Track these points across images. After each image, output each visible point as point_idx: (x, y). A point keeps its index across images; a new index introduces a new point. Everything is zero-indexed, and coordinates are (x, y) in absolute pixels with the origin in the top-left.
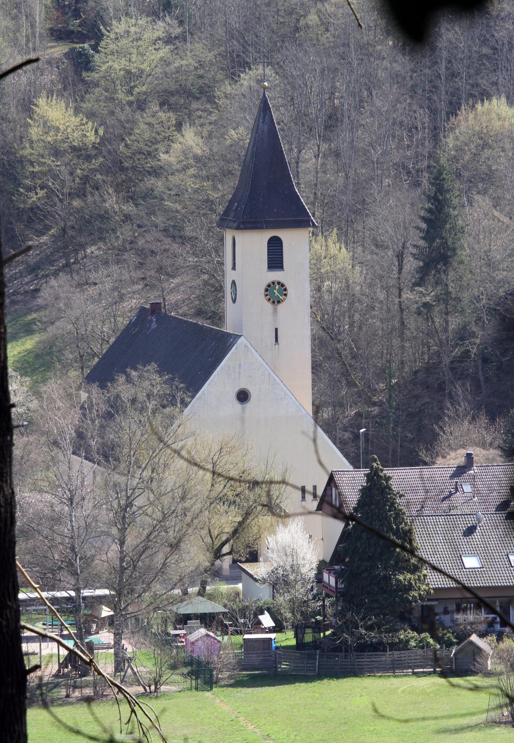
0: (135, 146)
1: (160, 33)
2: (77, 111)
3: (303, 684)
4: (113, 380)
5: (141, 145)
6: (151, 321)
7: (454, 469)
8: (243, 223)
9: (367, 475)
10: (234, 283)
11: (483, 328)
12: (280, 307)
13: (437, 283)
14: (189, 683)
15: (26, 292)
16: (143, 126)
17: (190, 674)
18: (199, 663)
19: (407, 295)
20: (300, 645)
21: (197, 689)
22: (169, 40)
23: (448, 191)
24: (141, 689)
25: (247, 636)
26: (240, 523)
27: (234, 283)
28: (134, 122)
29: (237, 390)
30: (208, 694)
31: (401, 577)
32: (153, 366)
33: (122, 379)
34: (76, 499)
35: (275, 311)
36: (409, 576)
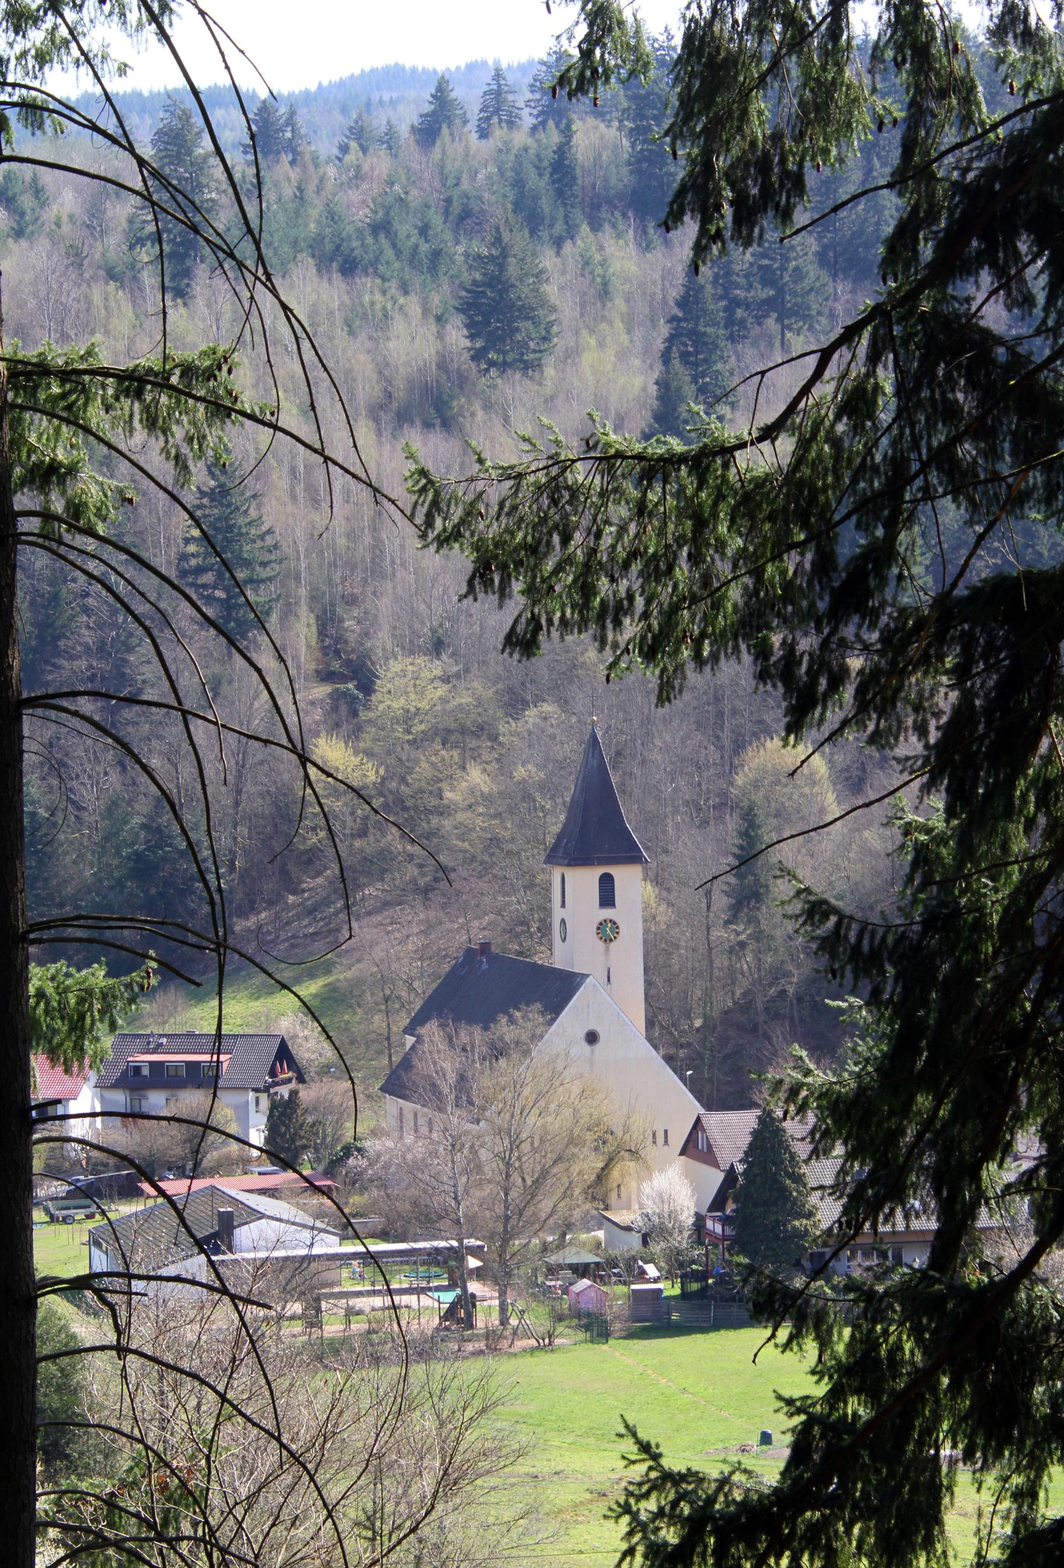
0: (416, 785)
1: (438, 672)
2: (356, 753)
3: (699, 1336)
4: (494, 1021)
5: (423, 784)
6: (481, 962)
7: (36, 1136)
8: (574, 859)
9: (759, 1117)
10: (563, 921)
11: (798, 967)
12: (612, 944)
13: (749, 922)
14: (581, 1335)
15: (305, 936)
16: (424, 765)
17: (579, 1327)
18: (589, 1315)
19: (719, 933)
20: (685, 1296)
21: (592, 1342)
22: (446, 679)
23: (759, 827)
24: (533, 1342)
25: (633, 1287)
26: (603, 1169)
27: (563, 921)
28: (417, 761)
29: (585, 1031)
30: (605, 1347)
31: (797, 1223)
32: (538, 1005)
33: (504, 1020)
34: (458, 1147)
35: (607, 949)
36: (805, 1222)
